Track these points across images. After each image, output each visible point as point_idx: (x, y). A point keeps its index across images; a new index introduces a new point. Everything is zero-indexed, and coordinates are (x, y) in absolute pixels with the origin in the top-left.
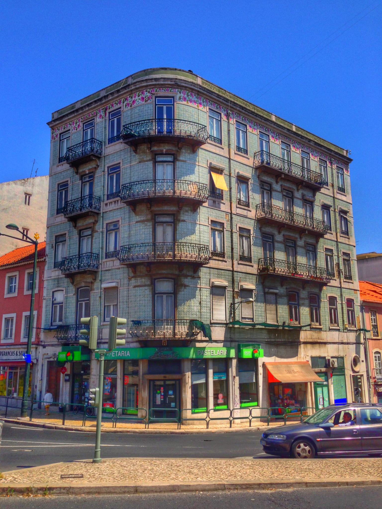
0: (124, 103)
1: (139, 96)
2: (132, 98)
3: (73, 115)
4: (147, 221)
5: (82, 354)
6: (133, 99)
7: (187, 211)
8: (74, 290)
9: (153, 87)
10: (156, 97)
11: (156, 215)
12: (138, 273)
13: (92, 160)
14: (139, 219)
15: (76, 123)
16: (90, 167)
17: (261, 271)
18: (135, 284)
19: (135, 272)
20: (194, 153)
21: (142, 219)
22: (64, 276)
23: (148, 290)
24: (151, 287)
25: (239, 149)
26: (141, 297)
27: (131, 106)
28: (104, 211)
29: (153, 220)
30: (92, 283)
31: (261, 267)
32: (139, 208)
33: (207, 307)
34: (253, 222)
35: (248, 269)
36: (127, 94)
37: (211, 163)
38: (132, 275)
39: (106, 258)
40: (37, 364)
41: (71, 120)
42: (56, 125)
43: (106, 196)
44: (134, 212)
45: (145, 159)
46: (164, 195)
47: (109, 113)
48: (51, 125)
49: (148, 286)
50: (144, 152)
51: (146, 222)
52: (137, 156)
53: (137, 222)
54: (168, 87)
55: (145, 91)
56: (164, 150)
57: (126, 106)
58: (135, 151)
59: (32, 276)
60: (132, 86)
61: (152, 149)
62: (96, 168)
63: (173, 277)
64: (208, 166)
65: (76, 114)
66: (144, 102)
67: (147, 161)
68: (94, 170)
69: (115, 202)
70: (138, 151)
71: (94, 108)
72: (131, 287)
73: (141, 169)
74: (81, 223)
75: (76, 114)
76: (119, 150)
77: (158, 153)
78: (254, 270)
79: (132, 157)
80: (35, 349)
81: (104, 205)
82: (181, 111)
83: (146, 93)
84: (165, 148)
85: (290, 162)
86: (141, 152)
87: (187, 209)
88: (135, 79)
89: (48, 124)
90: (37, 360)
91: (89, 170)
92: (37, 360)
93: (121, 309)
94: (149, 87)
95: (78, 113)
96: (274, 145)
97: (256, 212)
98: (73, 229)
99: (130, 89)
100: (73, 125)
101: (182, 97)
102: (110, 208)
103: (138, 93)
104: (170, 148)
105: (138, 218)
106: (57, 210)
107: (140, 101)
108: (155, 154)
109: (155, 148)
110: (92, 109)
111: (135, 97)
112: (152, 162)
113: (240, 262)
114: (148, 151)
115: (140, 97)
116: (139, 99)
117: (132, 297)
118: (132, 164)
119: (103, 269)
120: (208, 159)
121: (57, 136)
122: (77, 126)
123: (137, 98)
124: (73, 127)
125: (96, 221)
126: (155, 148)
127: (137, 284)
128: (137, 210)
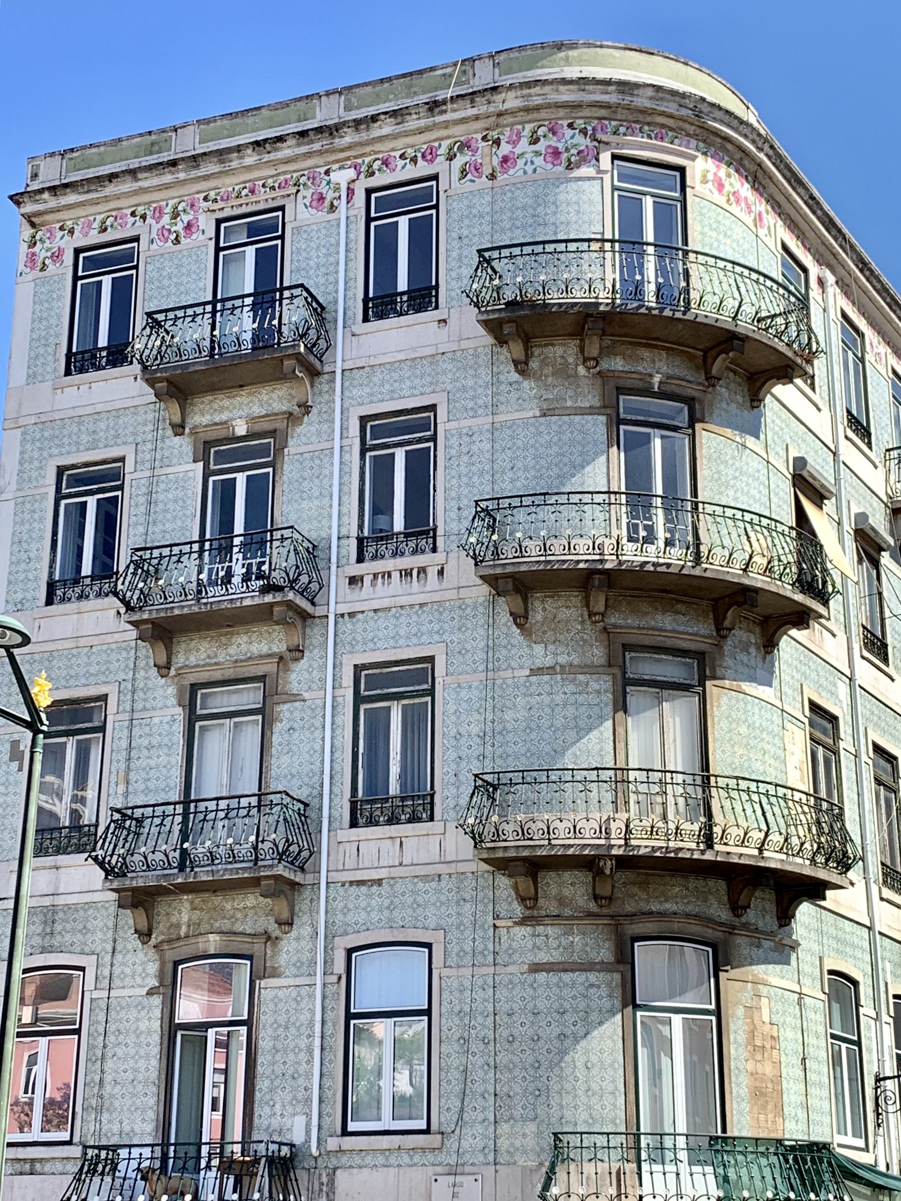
0: (451, 158)
1: (535, 141)
3: (168, 178)
4: (588, 669)
6: (505, 149)
8: (153, 968)
9: (603, 113)
11: (627, 647)
12: (548, 906)
13: (289, 377)
14: (549, 661)
15: (175, 215)
16: (257, 410)
18: (530, 958)
19: (529, 900)
20: (753, 407)
21: (563, 659)
23: (604, 991)
24: (617, 976)
26: (570, 1018)
27: (492, 177)
28: (343, 609)
29: (617, 671)
32: (541, 610)
36: (561, 113)
39: (354, 824)
41: (146, 198)
43: (354, 543)
45: (569, 403)
46: (620, 563)
47: (369, 192)
48: (29, 208)
49: (603, 967)
50: (564, 372)
51: (582, 677)
52: (526, 384)
53: (537, 671)
54: (663, 126)
55: (565, 123)
56: (657, 379)
57: (464, 173)
58: (522, 367)
60: (511, 94)
61: (605, 365)
63: (710, 933)
65: (182, 176)
66: (560, 169)
68: (280, 425)
69: (407, 573)
70: (534, 364)
71: (288, 161)
73: (549, 445)
74: (198, 655)
75: (182, 176)
76: (430, 351)
77: (628, 384)
79: (504, 388)
83: (569, 133)
86: (548, 370)
88: (509, 71)
89: (16, 199)
91: (252, 420)
93: (454, 1075)
94: (586, 112)
95: (194, 173)
101: (710, 176)
102: (371, 596)
103: (529, 127)
104: (677, 372)
105: (541, 655)
106: (51, 587)
107: (539, 161)
108: (614, 390)
109: (617, 364)
110: (275, 163)
111: (515, 143)
112: (603, 419)
114: (581, 370)
115: (541, 146)
116: (537, 153)
119: (334, 877)
120: (789, 441)
121: (57, 256)
122: (179, 227)
124: (156, 227)
126: (617, 364)
127: (543, 957)
128: (537, 616)
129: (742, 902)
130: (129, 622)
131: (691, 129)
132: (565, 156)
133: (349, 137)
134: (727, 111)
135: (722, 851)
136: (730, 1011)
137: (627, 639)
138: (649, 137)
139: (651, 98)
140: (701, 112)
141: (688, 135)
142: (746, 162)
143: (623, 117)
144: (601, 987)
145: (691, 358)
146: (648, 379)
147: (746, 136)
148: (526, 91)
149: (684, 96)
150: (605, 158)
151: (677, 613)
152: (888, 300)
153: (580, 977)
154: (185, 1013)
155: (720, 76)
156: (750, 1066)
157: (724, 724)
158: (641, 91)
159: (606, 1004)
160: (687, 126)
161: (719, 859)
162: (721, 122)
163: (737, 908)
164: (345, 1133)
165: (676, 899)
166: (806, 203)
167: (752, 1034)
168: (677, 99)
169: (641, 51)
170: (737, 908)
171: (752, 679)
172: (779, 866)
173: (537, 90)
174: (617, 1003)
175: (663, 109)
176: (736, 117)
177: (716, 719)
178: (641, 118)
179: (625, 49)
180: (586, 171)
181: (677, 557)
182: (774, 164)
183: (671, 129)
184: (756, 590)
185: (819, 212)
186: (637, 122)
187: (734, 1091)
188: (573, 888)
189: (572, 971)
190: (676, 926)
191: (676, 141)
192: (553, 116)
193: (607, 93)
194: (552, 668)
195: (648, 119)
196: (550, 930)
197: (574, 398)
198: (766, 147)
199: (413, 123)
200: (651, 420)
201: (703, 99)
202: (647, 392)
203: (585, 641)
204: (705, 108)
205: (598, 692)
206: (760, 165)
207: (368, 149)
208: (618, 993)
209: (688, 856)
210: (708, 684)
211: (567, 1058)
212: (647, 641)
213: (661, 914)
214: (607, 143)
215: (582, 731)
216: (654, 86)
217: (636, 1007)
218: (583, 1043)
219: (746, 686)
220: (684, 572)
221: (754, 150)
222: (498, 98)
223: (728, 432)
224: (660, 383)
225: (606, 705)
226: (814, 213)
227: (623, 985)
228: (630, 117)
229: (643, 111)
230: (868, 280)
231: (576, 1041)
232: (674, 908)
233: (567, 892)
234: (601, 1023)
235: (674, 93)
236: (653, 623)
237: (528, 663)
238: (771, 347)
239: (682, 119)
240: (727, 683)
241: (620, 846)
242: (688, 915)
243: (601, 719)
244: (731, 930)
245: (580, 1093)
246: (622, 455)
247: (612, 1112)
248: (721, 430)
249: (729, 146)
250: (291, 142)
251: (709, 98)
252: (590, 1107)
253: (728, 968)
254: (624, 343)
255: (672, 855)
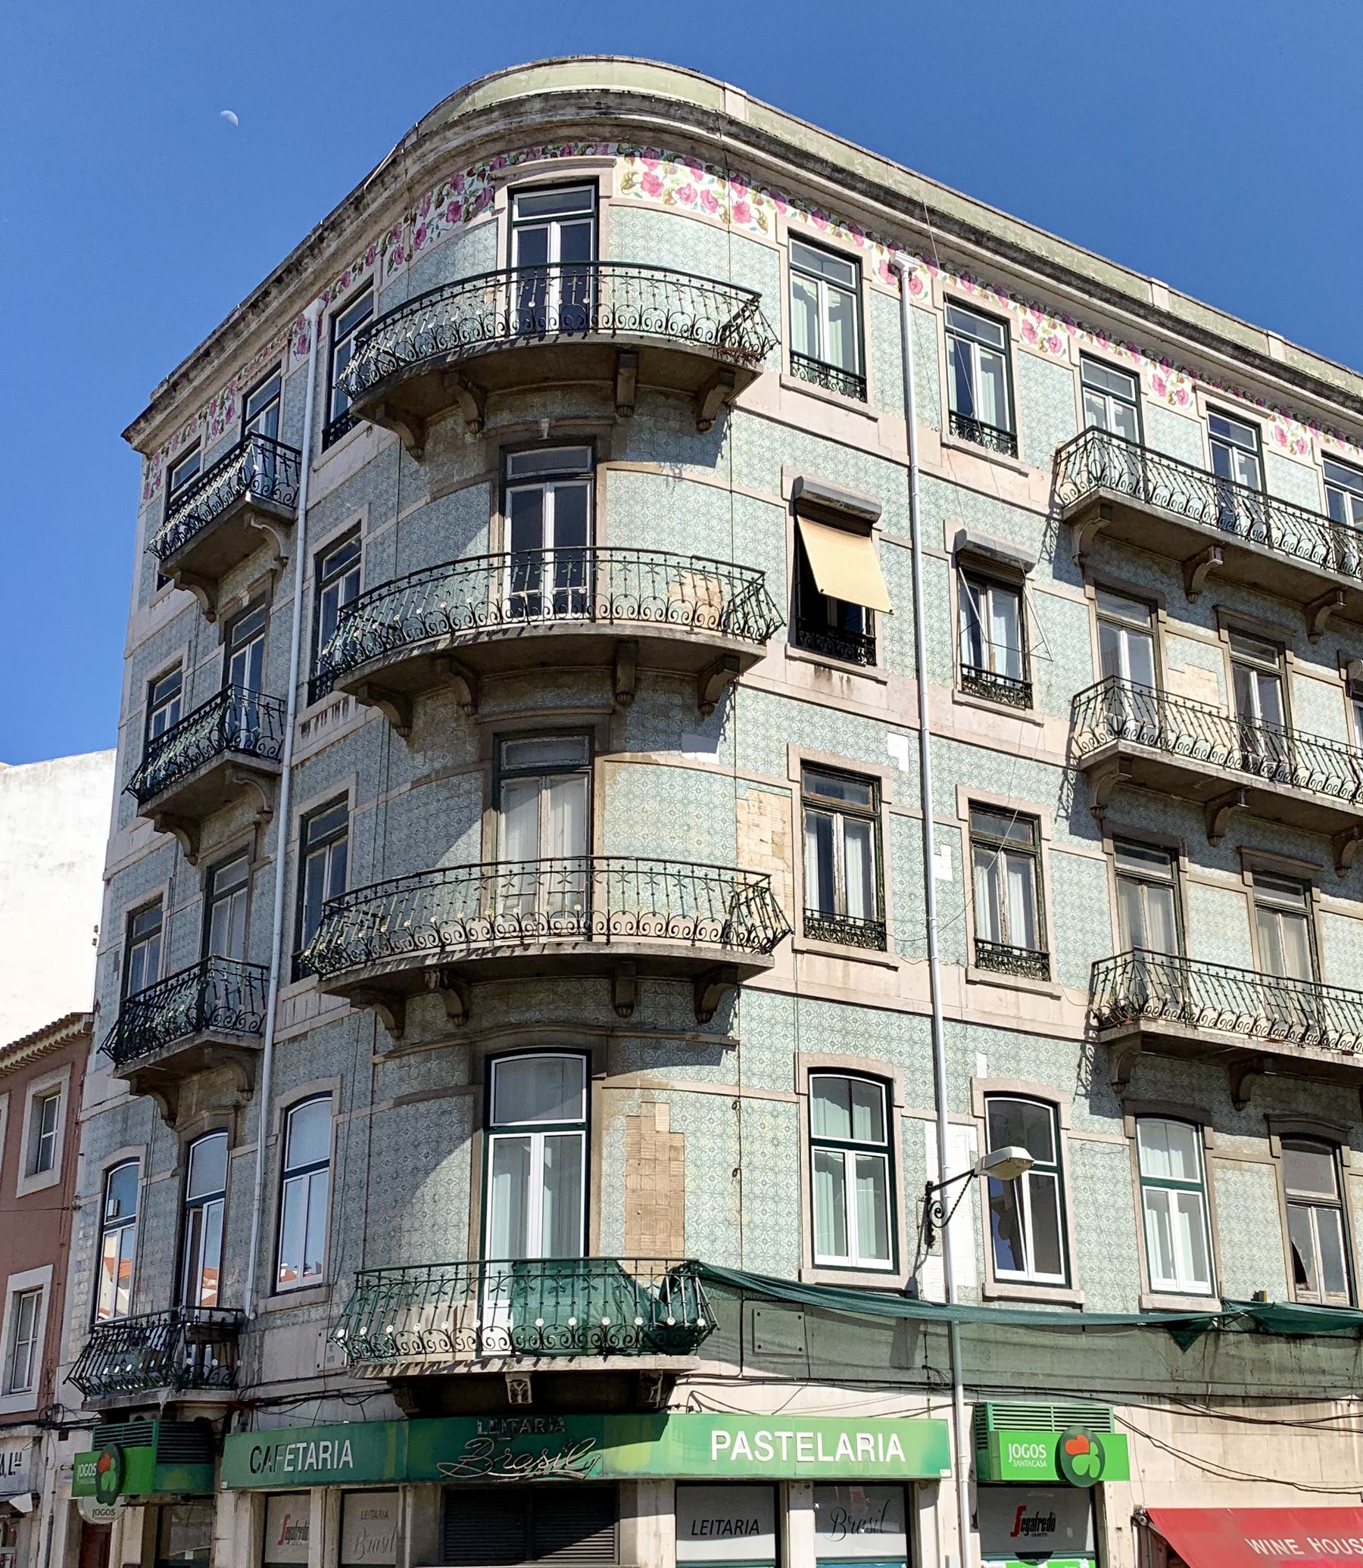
1: (439, 204)
2: (414, 220)
3: (208, 370)
4: (461, 770)
5: (162, 1459)
6: (420, 220)
7: (664, 712)
9: (499, 146)
10: (511, 192)
12: (413, 1034)
17: (1103, 1024)
19: (399, 1028)
20: (701, 431)
22: (125, 1085)
24: (469, 1099)
25: (965, 422)
30: (238, 1107)
31: (1103, 1004)
33: (776, 1199)
34: (1055, 777)
35: (1031, 1010)
36: (460, 161)
37: (798, 482)
38: (388, 1042)
40: (34, 1517)
41: (205, 396)
42: (154, 435)
44: (405, 736)
49: (458, 1091)
50: (455, 446)
51: (454, 780)
54: (569, 138)
55: (465, 172)
56: (545, 425)
59: (45, 1105)
62: (275, 575)
63: (579, 1040)
64: (788, 495)
66: (459, 223)
67: (466, 484)
72: (383, 1106)
78: (1071, 1016)
80: (30, 1443)
81: (299, 730)
82: (635, 235)
84: (545, 414)
85: (1264, 493)
87: (661, 699)
90: (36, 1498)
92: (36, 1498)
96: (1166, 420)
97: (1072, 729)
98: (184, 864)
99: (405, 179)
100: (212, 413)
105: (420, 764)
107: (443, 223)
111: (424, 214)
112: (486, 486)
113: (977, 974)
115: (444, 208)
116: (441, 215)
117: (384, 1158)
118: (403, 515)
120: (789, 462)
123: (433, 212)
125: (262, 812)
127: (405, 1089)
129: (706, 1004)
130: (143, 815)
131: (606, 131)
132: (463, 209)
133: (311, 267)
134: (643, 97)
135: (598, 944)
136: (605, 1123)
137: (496, 728)
138: (554, 155)
139: (542, 111)
140: (609, 107)
141: (605, 139)
142: (703, 150)
143: (521, 143)
144: (456, 1110)
145: (593, 390)
146: (535, 427)
147: (684, 120)
148: (419, 152)
149: (579, 95)
150: (501, 197)
151: (560, 687)
152: (1049, 270)
153: (433, 1105)
154: (1246, 1295)
155: (663, 61)
156: (632, 1182)
157: (620, 803)
158: (527, 107)
159: (457, 1130)
160: (600, 130)
161: (546, 952)
162: (641, 111)
163: (624, 1008)
164: (274, 1293)
165: (541, 1007)
166: (829, 178)
167: (637, 1146)
168: (573, 101)
169: (551, 64)
170: (624, 1008)
171: (669, 746)
172: (632, 951)
173: (428, 146)
174: (468, 1128)
175: (558, 118)
176: (659, 100)
177: (608, 799)
178: (541, 138)
179: (532, 68)
180: (484, 216)
181: (572, 621)
182: (747, 143)
183: (582, 139)
184: (634, 640)
185: (859, 185)
186: (537, 144)
187: (604, 1212)
188: (430, 1012)
189: (427, 1100)
190: (537, 1035)
191: (588, 151)
192: (454, 168)
193: (493, 122)
194: (428, 776)
195: (551, 137)
196: (412, 1059)
197: (460, 471)
198: (723, 125)
199: (350, 229)
200: (543, 473)
201: (606, 92)
202: (535, 442)
203: (458, 739)
204: (610, 101)
205: (469, 792)
206: (726, 149)
207: (330, 274)
208: (469, 1117)
209: (507, 953)
210: (598, 760)
211: (418, 1193)
212: (522, 725)
213: (519, 1025)
214: (503, 178)
215: (451, 839)
216: (539, 95)
217: (488, 1130)
218: (433, 1175)
219: (655, 756)
220: (525, 634)
221: (704, 133)
222: (400, 169)
223: (651, 466)
224: (550, 428)
225: (476, 805)
226: (853, 189)
227: (475, 1107)
228: (529, 141)
229: (541, 129)
230: (996, 252)
231: (427, 1174)
232: (538, 1016)
233: (428, 1017)
234: (450, 1152)
235: (567, 96)
236: (531, 704)
237: (411, 777)
238: (676, 351)
239: (588, 123)
240: (627, 756)
241: (434, 955)
242: (555, 1022)
243: (471, 821)
244: (610, 1032)
245: (427, 1229)
246: (508, 522)
247: (457, 1244)
248: (637, 465)
249: (666, 137)
250: (274, 292)
251: (614, 88)
252: (434, 1243)
253: (604, 1075)
254: (511, 394)
255: (489, 955)
